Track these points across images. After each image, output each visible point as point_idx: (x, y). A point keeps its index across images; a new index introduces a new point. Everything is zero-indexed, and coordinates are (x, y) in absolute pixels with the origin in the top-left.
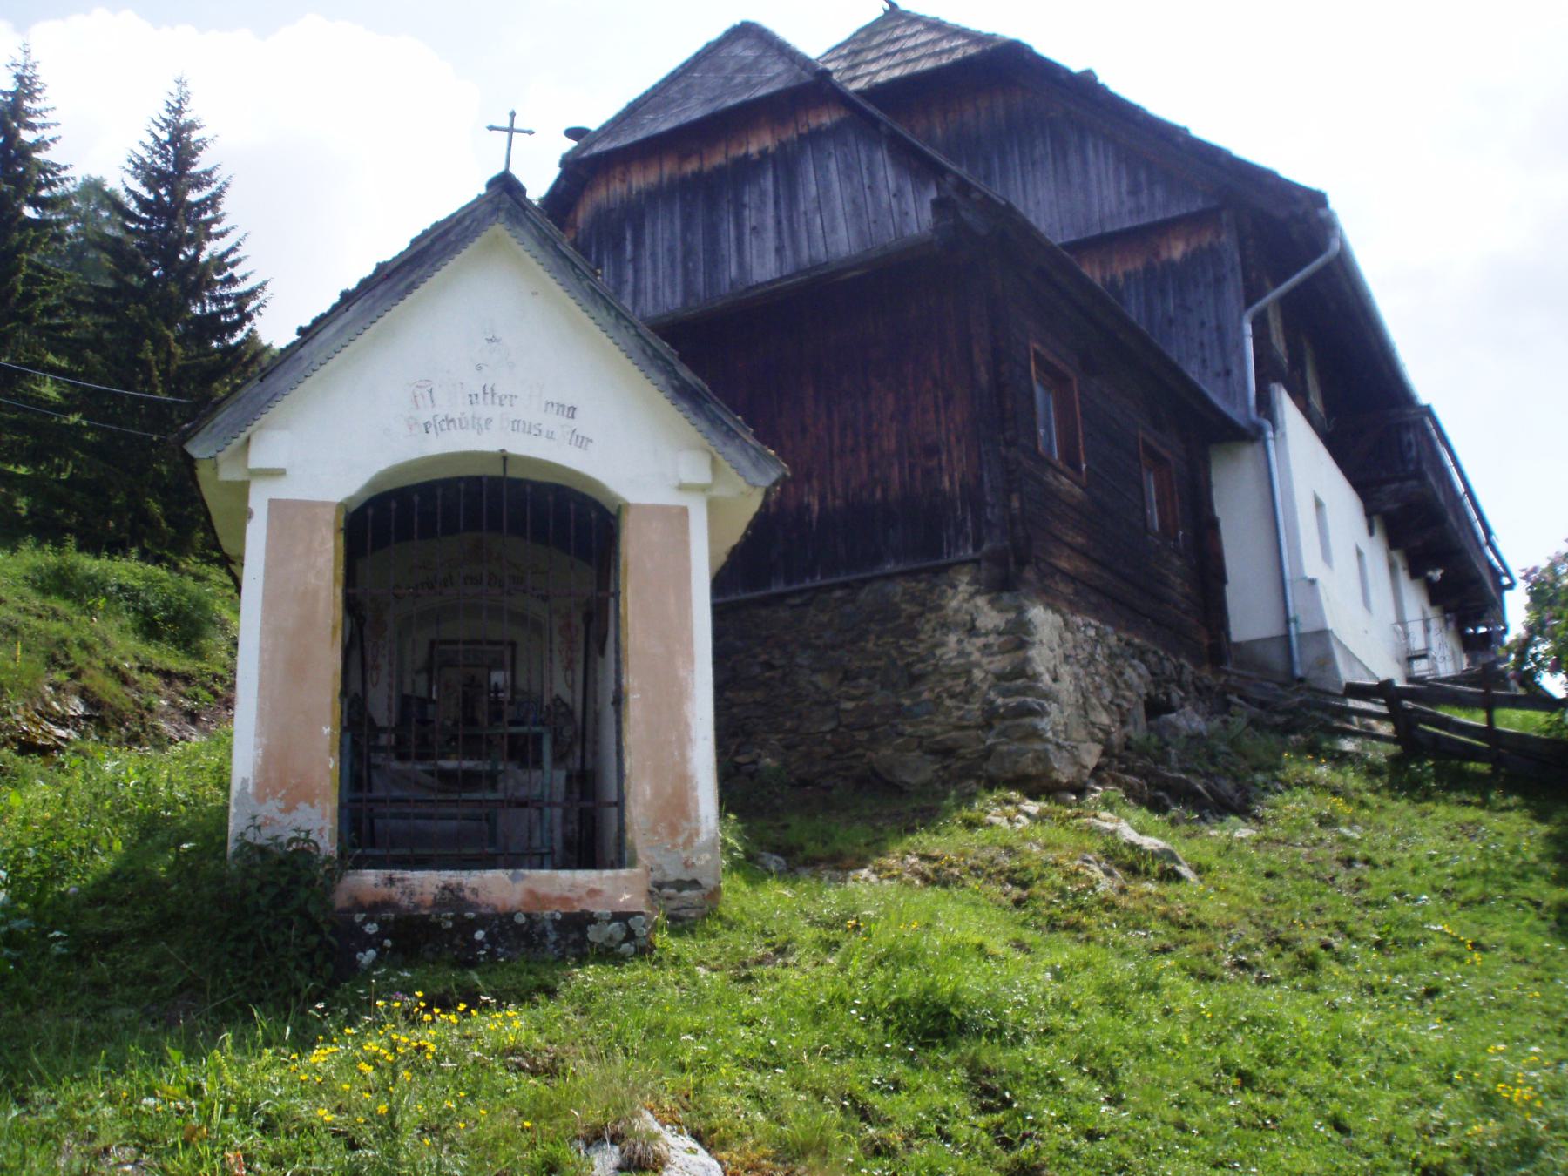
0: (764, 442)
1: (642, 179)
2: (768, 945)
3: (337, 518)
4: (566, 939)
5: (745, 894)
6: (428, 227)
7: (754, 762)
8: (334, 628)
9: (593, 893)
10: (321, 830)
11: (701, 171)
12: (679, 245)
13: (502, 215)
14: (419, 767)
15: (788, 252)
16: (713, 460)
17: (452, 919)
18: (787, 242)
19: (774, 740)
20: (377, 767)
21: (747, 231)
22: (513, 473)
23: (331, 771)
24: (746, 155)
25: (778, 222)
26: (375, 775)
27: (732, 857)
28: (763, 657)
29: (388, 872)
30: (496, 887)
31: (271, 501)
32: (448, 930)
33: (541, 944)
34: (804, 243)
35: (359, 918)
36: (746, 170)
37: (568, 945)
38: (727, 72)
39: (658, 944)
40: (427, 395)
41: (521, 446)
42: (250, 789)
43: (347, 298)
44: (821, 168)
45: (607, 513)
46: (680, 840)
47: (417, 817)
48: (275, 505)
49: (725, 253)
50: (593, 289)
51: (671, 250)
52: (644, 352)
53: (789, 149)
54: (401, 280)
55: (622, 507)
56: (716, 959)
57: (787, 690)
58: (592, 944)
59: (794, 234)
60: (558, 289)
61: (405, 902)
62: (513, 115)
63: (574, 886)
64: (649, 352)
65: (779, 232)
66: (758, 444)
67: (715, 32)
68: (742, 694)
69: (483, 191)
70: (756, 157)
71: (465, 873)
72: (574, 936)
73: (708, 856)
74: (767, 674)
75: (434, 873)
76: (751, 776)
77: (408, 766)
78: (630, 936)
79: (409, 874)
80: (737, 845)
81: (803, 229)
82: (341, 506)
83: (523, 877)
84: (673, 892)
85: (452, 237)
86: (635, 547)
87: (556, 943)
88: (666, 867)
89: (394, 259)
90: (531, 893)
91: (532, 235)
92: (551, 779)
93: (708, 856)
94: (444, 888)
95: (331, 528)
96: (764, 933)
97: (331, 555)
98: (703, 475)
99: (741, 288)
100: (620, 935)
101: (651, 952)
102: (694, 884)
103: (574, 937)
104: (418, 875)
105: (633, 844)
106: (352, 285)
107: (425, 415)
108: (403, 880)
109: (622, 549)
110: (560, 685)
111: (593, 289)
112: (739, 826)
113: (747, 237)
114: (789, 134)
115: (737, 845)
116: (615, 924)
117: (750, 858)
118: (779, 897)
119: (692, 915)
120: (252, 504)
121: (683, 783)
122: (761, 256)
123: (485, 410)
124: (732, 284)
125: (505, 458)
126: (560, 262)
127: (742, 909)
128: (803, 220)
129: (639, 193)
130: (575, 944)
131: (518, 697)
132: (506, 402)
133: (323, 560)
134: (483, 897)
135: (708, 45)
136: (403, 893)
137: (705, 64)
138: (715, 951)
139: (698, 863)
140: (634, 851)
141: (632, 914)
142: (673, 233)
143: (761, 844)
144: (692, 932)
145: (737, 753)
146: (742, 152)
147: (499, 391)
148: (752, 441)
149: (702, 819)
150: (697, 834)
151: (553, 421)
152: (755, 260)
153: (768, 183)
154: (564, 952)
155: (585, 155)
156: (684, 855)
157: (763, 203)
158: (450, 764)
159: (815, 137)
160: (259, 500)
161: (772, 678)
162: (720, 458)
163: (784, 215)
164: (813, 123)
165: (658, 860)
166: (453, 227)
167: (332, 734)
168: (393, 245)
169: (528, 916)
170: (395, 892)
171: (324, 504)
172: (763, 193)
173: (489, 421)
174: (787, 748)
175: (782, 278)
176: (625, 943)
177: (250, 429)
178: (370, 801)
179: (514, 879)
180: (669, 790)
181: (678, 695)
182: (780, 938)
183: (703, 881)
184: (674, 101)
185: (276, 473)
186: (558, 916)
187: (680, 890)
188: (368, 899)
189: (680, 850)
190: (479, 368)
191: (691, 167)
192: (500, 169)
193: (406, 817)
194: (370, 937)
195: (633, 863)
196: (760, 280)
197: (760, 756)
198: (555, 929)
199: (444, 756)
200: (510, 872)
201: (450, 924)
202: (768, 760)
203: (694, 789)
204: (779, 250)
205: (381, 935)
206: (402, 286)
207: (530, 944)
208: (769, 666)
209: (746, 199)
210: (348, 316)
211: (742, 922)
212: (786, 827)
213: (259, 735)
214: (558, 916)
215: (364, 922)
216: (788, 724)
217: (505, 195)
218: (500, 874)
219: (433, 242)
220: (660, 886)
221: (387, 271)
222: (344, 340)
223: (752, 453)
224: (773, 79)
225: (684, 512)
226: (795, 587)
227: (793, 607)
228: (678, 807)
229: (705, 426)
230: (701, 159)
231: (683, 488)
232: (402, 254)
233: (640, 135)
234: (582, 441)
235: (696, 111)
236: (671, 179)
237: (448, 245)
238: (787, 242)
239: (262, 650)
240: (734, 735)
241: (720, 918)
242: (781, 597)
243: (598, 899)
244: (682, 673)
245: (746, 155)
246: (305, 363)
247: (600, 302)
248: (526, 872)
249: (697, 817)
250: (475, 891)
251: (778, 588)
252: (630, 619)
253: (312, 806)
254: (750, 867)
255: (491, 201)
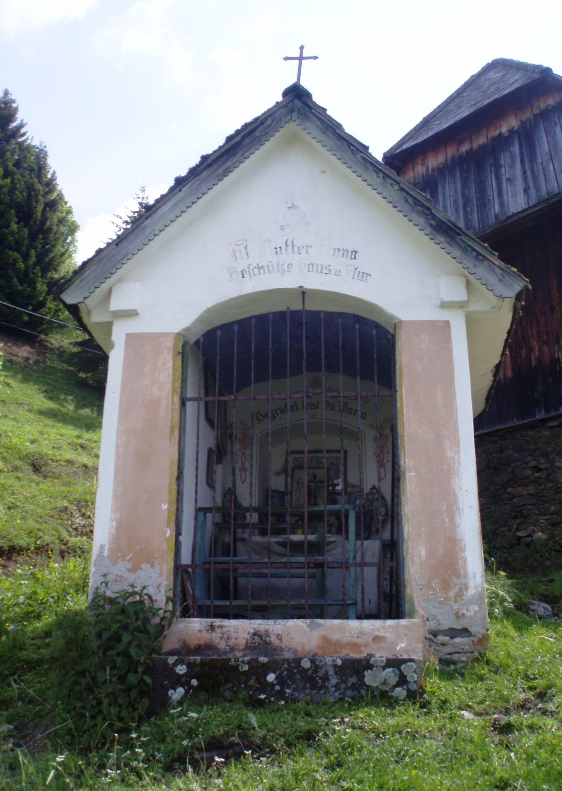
0: (506, 262)
1: (435, 161)
2: (530, 688)
3: (175, 344)
4: (346, 682)
5: (513, 638)
6: (239, 127)
7: (530, 536)
8: (172, 428)
9: (377, 639)
10: (159, 586)
11: (471, 149)
12: (460, 197)
13: (295, 115)
14: (274, 540)
15: (532, 191)
16: (468, 283)
17: (249, 663)
18: (531, 184)
19: (542, 520)
20: (243, 540)
21: (504, 182)
22: (311, 306)
23: (168, 539)
24: (500, 134)
25: (524, 173)
26: (239, 544)
27: (504, 607)
28: (533, 463)
29: (210, 620)
30: (297, 635)
31: (127, 335)
32: (245, 672)
33: (324, 687)
34: (543, 183)
35: (171, 660)
36: (500, 143)
37: (347, 689)
38: (484, 88)
39: (428, 689)
40: (244, 249)
41: (314, 282)
42: (106, 554)
43: (180, 182)
44: (550, 133)
45: (387, 332)
46: (451, 594)
47: (273, 576)
48: (130, 338)
49: (491, 198)
50: (364, 159)
51: (455, 202)
52: (407, 201)
53: (528, 125)
54: (220, 166)
55: (397, 324)
56: (481, 702)
57: (550, 485)
58: (368, 687)
59: (535, 178)
60: (339, 163)
61: (222, 645)
62: (302, 48)
63: (361, 633)
64: (410, 200)
65: (525, 179)
66: (503, 265)
67: (476, 69)
68: (520, 489)
69: (280, 99)
70: (507, 134)
71: (271, 622)
72: (353, 680)
73: (476, 608)
74: (536, 475)
75: (246, 621)
76: (528, 545)
77: (266, 539)
78: (403, 681)
79: (226, 622)
80: (507, 596)
81: (541, 172)
82: (178, 335)
83: (319, 625)
84: (447, 638)
85: (257, 133)
86: (409, 360)
87: (337, 686)
88: (439, 617)
89: (215, 152)
90: (325, 639)
91: (317, 126)
92: (373, 548)
93: (476, 608)
94: (255, 634)
95: (171, 353)
96: (527, 678)
97: (171, 372)
98: (461, 295)
99: (503, 218)
100: (394, 680)
101: (421, 695)
102: (465, 632)
103: (354, 684)
104: (234, 622)
105: (411, 596)
106: (183, 173)
107: (242, 265)
108: (221, 627)
109: (398, 358)
110: (371, 478)
111: (364, 159)
112: (509, 582)
113: (504, 185)
114: (527, 115)
115: (507, 596)
116: (391, 669)
117: (521, 607)
118: (542, 642)
119: (464, 659)
120: (114, 338)
121: (454, 545)
122: (514, 195)
123: (286, 258)
124: (496, 216)
125: (303, 293)
126: (338, 143)
127: (509, 655)
128: (540, 167)
129: (433, 170)
130: (354, 687)
131: (349, 489)
132: (303, 251)
133: (164, 376)
134: (285, 643)
135: (472, 76)
136: (221, 638)
137: (471, 88)
138: (481, 694)
139: (467, 614)
140: (413, 604)
141: (405, 661)
142: (456, 191)
143: (532, 594)
144: (462, 675)
145: (518, 530)
146: (497, 132)
147: (297, 243)
148: (498, 262)
149: (470, 575)
150: (467, 589)
151: (341, 263)
152: (510, 199)
153: (516, 148)
154: (343, 694)
155: (398, 151)
156: (455, 607)
157: (513, 162)
158: (297, 537)
159: (545, 115)
160: (119, 334)
161: (539, 478)
162: (471, 278)
163: (527, 167)
164: (543, 106)
165: (433, 611)
166: (258, 127)
167: (169, 509)
168: (213, 142)
169: (312, 661)
170: (215, 637)
171: (166, 335)
172: (512, 157)
173: (290, 265)
174: (553, 525)
175: (530, 208)
176: (402, 688)
177: (109, 282)
178: (235, 563)
179: (310, 626)
180: (441, 551)
181: (446, 473)
182: (541, 683)
183: (472, 629)
184: (451, 111)
185: (131, 314)
186: (339, 662)
187: (452, 638)
188: (193, 643)
189: (452, 602)
190: (282, 228)
191: (465, 148)
192: (293, 81)
193: (264, 576)
194: (180, 676)
195: (411, 615)
196: (515, 212)
197: (534, 531)
198: (336, 673)
199: (293, 532)
200: (309, 621)
201: (246, 668)
202: (540, 534)
203: (463, 550)
204: (526, 191)
205: (189, 676)
206: (220, 171)
207: (314, 686)
208: (538, 469)
209: (502, 162)
210: (180, 195)
211: (508, 666)
212: (552, 581)
213: (114, 511)
214: (339, 662)
215: (176, 664)
216: (553, 508)
217: (297, 102)
218: (300, 622)
219: (243, 138)
220: (435, 634)
221: (209, 161)
222: (177, 212)
223: (498, 271)
224: (515, 81)
225: (447, 324)
226: (553, 414)
227: (551, 428)
228: (448, 565)
229: (457, 252)
230: (471, 142)
231: (444, 305)
232: (220, 148)
233: (431, 134)
234: (363, 276)
235: (465, 112)
236: (453, 157)
237: (254, 141)
238: (531, 184)
239: (117, 446)
240: (515, 517)
241: (488, 663)
242: (543, 421)
243: (382, 644)
244: (449, 454)
245: (500, 134)
246: (149, 230)
247: (371, 168)
248: (321, 621)
249: (466, 574)
250: (279, 637)
251: (540, 415)
252: (405, 412)
253: (153, 566)
254: (520, 614)
255: (285, 106)
